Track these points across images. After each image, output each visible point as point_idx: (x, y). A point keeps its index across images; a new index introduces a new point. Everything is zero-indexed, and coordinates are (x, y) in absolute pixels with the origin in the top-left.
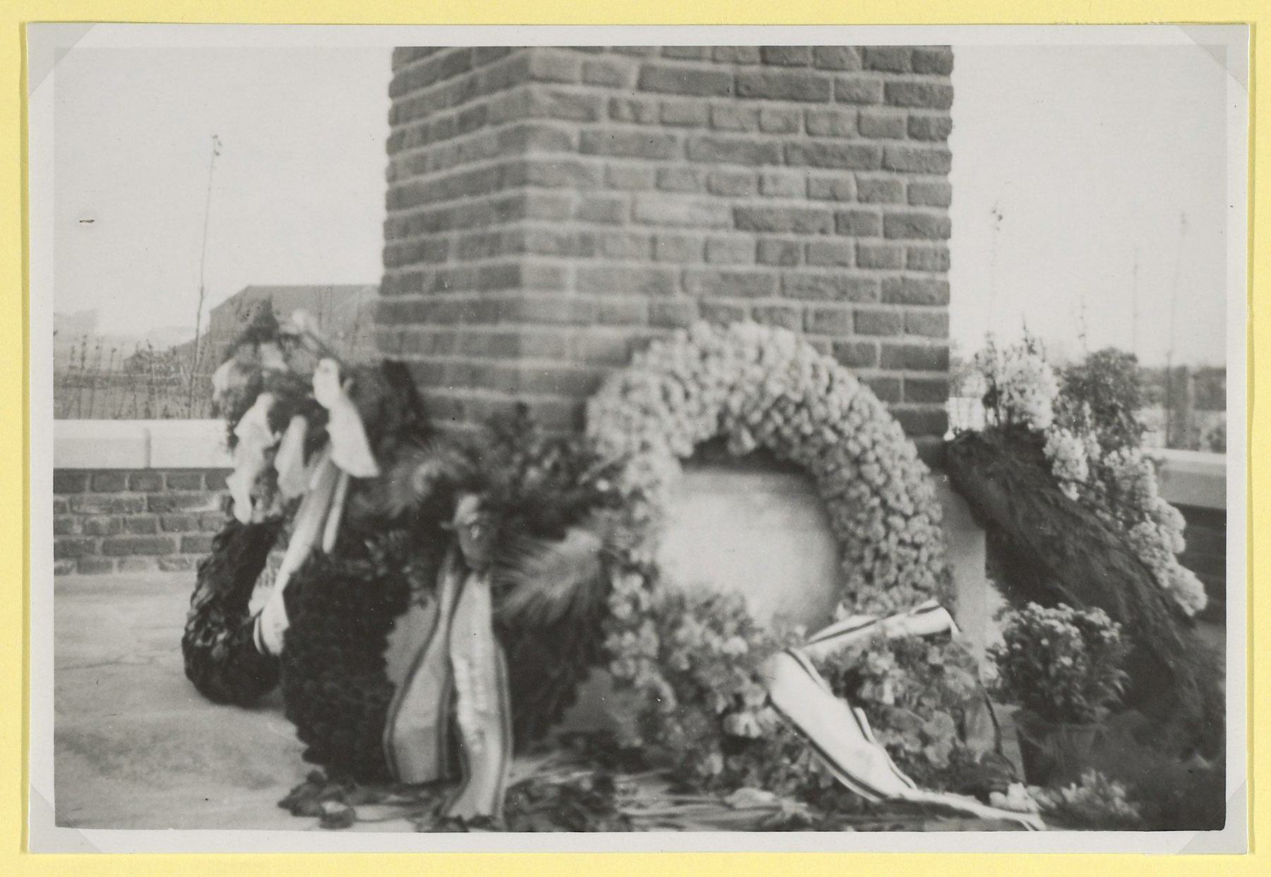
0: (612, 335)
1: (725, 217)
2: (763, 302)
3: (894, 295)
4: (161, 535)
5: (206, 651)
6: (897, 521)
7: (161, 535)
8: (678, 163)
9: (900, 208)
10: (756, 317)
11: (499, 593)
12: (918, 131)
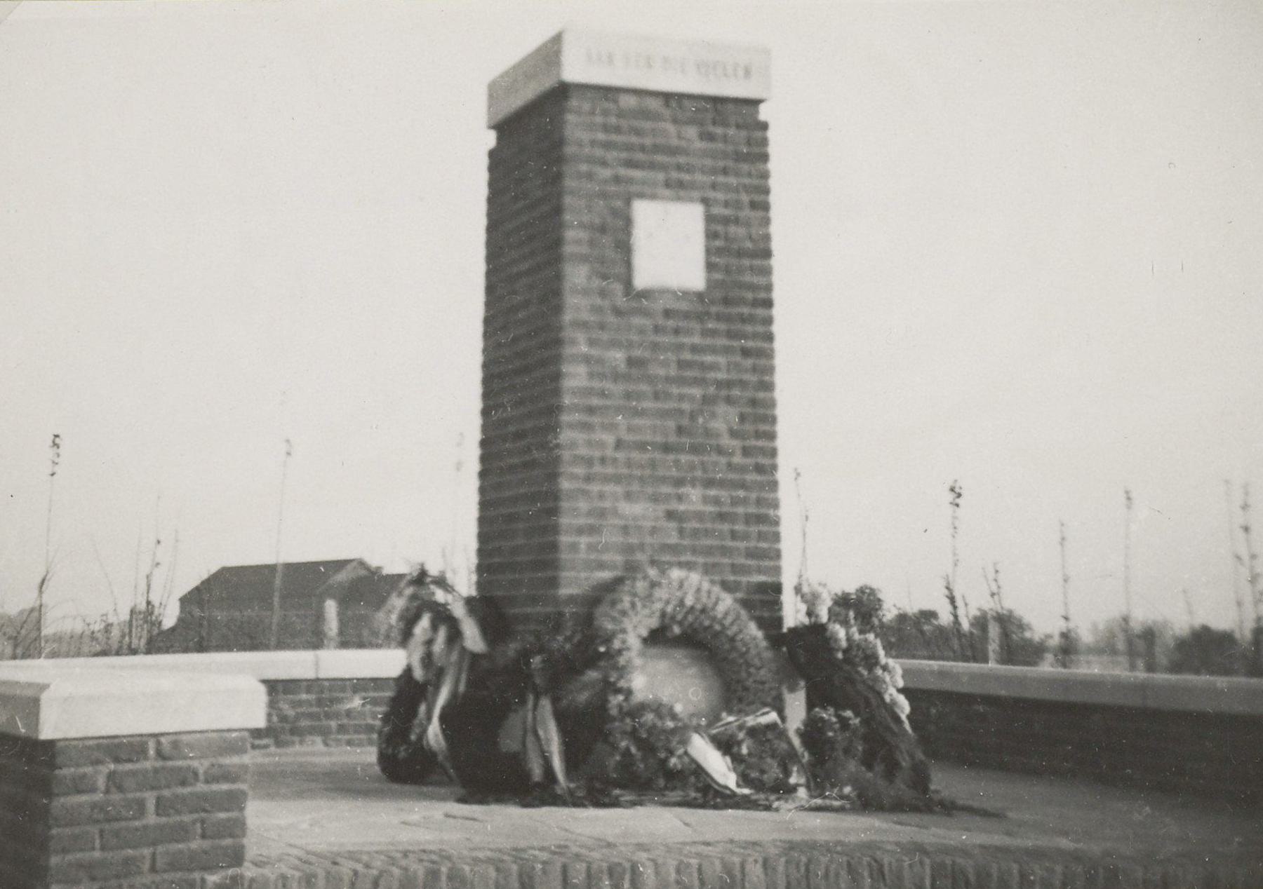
0: (606, 575)
1: (661, 514)
2: (683, 559)
3: (751, 554)
4: (325, 722)
5: (394, 756)
6: (752, 670)
7: (325, 722)
8: (635, 487)
9: (752, 510)
10: (681, 565)
11: (555, 701)
12: (759, 469)
